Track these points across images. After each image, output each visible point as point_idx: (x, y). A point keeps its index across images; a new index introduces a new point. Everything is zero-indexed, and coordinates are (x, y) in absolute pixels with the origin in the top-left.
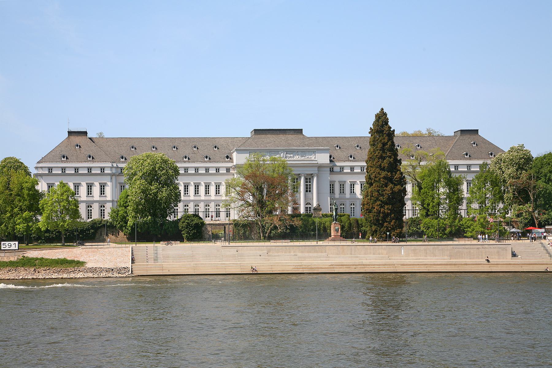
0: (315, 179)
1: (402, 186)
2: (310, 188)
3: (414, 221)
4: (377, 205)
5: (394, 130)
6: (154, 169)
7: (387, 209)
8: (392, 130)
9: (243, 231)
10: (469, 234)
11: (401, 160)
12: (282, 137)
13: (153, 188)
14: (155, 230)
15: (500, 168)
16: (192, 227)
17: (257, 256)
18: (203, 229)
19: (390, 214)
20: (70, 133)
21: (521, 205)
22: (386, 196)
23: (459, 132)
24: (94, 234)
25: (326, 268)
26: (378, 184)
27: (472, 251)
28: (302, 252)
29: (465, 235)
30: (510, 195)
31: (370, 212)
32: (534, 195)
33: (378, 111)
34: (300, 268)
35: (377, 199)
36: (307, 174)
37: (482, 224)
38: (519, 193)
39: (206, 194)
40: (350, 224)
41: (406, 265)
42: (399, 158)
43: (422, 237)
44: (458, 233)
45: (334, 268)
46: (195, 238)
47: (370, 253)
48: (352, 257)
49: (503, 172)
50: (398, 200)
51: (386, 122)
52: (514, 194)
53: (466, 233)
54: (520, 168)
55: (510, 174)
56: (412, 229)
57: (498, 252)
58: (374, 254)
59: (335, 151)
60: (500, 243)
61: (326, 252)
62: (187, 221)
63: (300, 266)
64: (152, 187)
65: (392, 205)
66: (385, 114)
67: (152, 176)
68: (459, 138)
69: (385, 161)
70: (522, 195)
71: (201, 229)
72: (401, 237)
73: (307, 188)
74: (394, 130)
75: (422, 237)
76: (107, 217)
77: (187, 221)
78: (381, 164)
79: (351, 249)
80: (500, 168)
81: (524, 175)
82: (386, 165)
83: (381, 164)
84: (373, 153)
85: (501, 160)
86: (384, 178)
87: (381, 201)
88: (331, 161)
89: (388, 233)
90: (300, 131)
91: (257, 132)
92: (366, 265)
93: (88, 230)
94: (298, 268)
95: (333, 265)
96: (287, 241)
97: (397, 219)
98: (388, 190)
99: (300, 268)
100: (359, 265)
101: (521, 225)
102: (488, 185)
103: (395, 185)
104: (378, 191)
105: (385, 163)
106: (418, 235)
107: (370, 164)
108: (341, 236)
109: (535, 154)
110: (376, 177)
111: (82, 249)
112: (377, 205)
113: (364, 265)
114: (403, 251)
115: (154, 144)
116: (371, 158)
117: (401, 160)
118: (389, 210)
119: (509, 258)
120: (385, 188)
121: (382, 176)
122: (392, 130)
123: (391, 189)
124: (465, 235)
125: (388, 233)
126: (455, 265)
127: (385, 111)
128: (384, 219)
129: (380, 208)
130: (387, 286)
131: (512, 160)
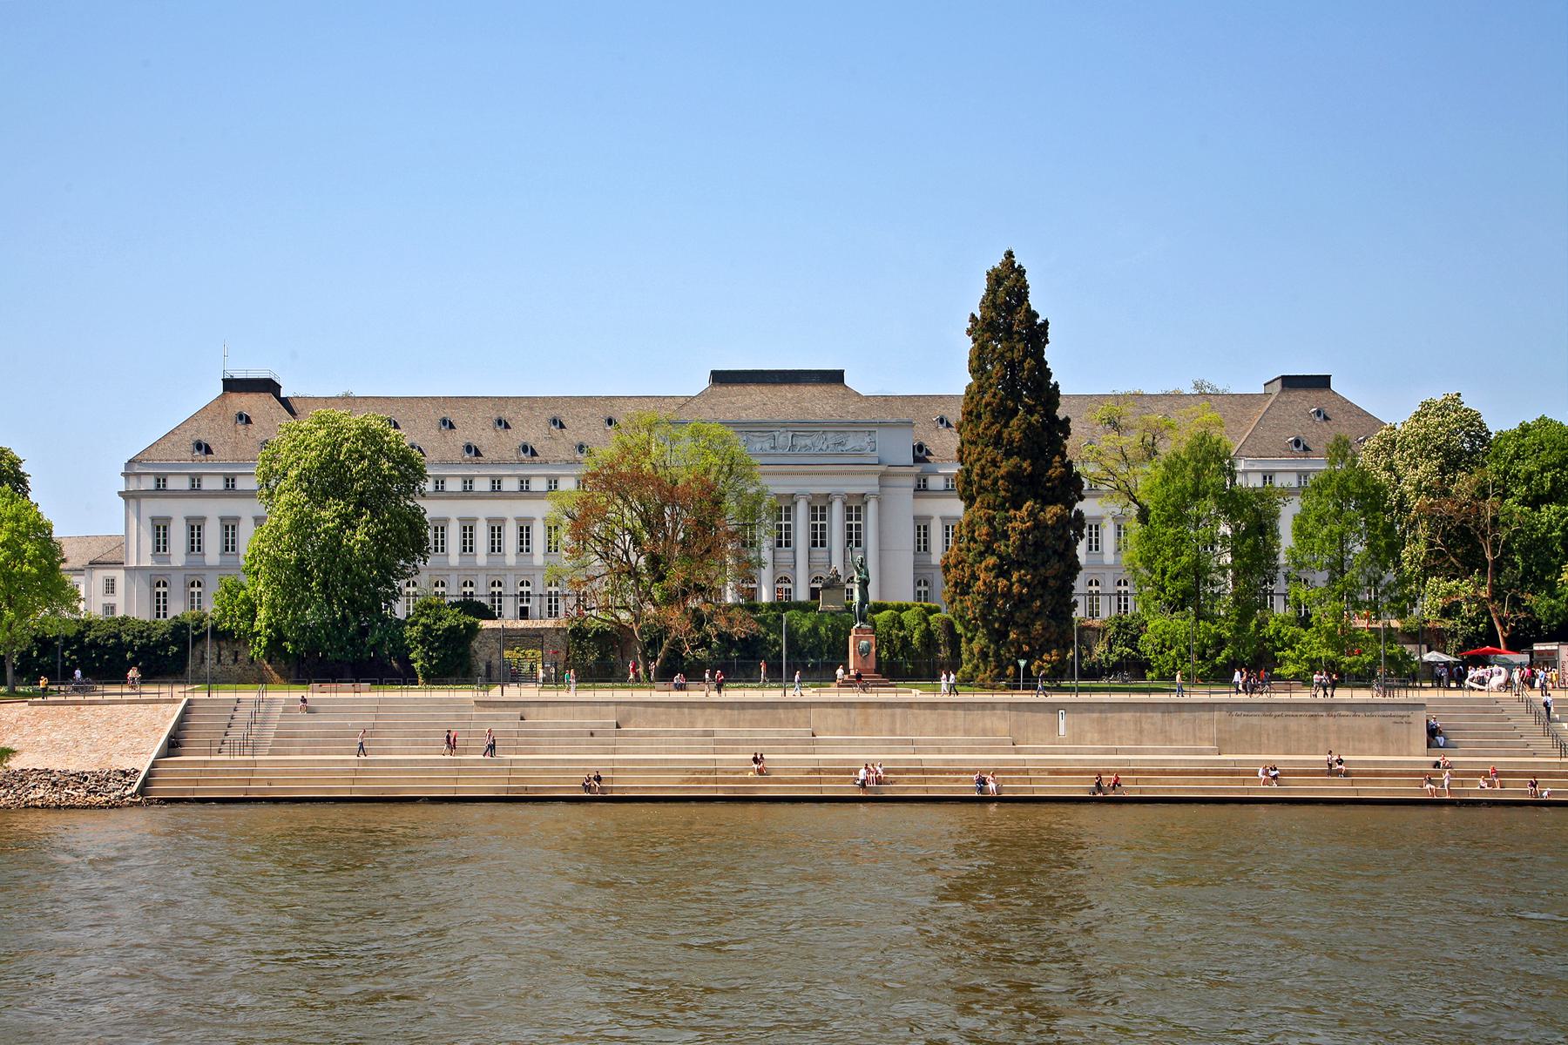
0: (872, 506)
1: (1070, 506)
2: (858, 536)
3: (1126, 626)
4: (987, 569)
5: (1046, 323)
6: (332, 458)
7: (1020, 580)
8: (1039, 321)
9: (597, 655)
10: (1291, 669)
11: (1067, 420)
12: (787, 391)
13: (328, 514)
14: (342, 649)
15: (1390, 468)
16: (438, 638)
17: (581, 734)
18: (475, 644)
19: (1032, 598)
20: (231, 385)
21: (1454, 577)
22: (1014, 538)
23: (1279, 383)
24: (181, 659)
25: (793, 781)
26: (991, 497)
27: (1293, 724)
28: (732, 724)
29: (1277, 671)
30: (1422, 548)
31: (964, 593)
32: (1495, 545)
33: (997, 261)
34: (706, 781)
35: (988, 550)
36: (850, 496)
37: (1330, 635)
38: (1446, 536)
39: (498, 542)
40: (928, 635)
41: (1069, 772)
42: (1061, 413)
43: (1144, 677)
44: (1261, 663)
45: (820, 781)
46: (448, 675)
47: (955, 730)
48: (892, 742)
49: (1399, 480)
50: (1051, 557)
51: (1021, 293)
52: (1431, 545)
53: (1279, 666)
54: (1453, 461)
55: (1420, 482)
56: (1118, 650)
57: (1382, 730)
58: (967, 732)
59: (935, 434)
60: (1388, 699)
61: (808, 723)
62: (423, 620)
63: (709, 772)
64: (325, 514)
65: (1035, 568)
66: (1021, 272)
67: (329, 479)
68: (1277, 400)
69: (1014, 422)
70: (1461, 546)
71: (468, 647)
72: (1058, 676)
73: (850, 536)
74: (1046, 323)
75: (1144, 677)
76: (211, 608)
77: (423, 620)
78: (1000, 433)
79: (893, 716)
80: (1390, 468)
81: (1464, 484)
82: (1017, 436)
83: (1000, 433)
84: (977, 398)
85: (1394, 443)
86: (1010, 476)
87: (1000, 557)
88: (917, 460)
89: (1022, 663)
90: (836, 377)
91: (719, 378)
92: (932, 772)
93: (163, 644)
94: (698, 781)
95: (819, 771)
96: (326, 686)
97: (1054, 615)
98: (1019, 520)
99: (706, 781)
100: (908, 771)
101: (1454, 644)
102: (1352, 510)
103: (1046, 502)
104: (990, 520)
105: (1014, 430)
106: (1134, 668)
107: (967, 435)
108: (878, 670)
109: (1499, 422)
110: (983, 476)
111: (31, 704)
112: (987, 569)
113: (923, 771)
114: (1062, 723)
115: (448, 414)
116: (970, 413)
117: (1067, 420)
118: (1027, 585)
119: (1419, 756)
120: (1012, 512)
121: (1002, 471)
122: (1039, 321)
123: (1032, 514)
124: (1277, 671)
125: (1022, 663)
126: (1232, 773)
127: (1018, 261)
128: (1022, 619)
129: (996, 577)
130: (1021, 845)
131: (1426, 438)
